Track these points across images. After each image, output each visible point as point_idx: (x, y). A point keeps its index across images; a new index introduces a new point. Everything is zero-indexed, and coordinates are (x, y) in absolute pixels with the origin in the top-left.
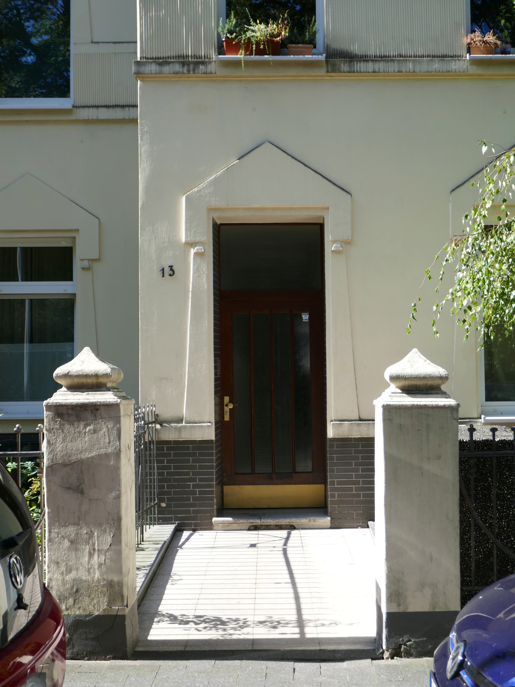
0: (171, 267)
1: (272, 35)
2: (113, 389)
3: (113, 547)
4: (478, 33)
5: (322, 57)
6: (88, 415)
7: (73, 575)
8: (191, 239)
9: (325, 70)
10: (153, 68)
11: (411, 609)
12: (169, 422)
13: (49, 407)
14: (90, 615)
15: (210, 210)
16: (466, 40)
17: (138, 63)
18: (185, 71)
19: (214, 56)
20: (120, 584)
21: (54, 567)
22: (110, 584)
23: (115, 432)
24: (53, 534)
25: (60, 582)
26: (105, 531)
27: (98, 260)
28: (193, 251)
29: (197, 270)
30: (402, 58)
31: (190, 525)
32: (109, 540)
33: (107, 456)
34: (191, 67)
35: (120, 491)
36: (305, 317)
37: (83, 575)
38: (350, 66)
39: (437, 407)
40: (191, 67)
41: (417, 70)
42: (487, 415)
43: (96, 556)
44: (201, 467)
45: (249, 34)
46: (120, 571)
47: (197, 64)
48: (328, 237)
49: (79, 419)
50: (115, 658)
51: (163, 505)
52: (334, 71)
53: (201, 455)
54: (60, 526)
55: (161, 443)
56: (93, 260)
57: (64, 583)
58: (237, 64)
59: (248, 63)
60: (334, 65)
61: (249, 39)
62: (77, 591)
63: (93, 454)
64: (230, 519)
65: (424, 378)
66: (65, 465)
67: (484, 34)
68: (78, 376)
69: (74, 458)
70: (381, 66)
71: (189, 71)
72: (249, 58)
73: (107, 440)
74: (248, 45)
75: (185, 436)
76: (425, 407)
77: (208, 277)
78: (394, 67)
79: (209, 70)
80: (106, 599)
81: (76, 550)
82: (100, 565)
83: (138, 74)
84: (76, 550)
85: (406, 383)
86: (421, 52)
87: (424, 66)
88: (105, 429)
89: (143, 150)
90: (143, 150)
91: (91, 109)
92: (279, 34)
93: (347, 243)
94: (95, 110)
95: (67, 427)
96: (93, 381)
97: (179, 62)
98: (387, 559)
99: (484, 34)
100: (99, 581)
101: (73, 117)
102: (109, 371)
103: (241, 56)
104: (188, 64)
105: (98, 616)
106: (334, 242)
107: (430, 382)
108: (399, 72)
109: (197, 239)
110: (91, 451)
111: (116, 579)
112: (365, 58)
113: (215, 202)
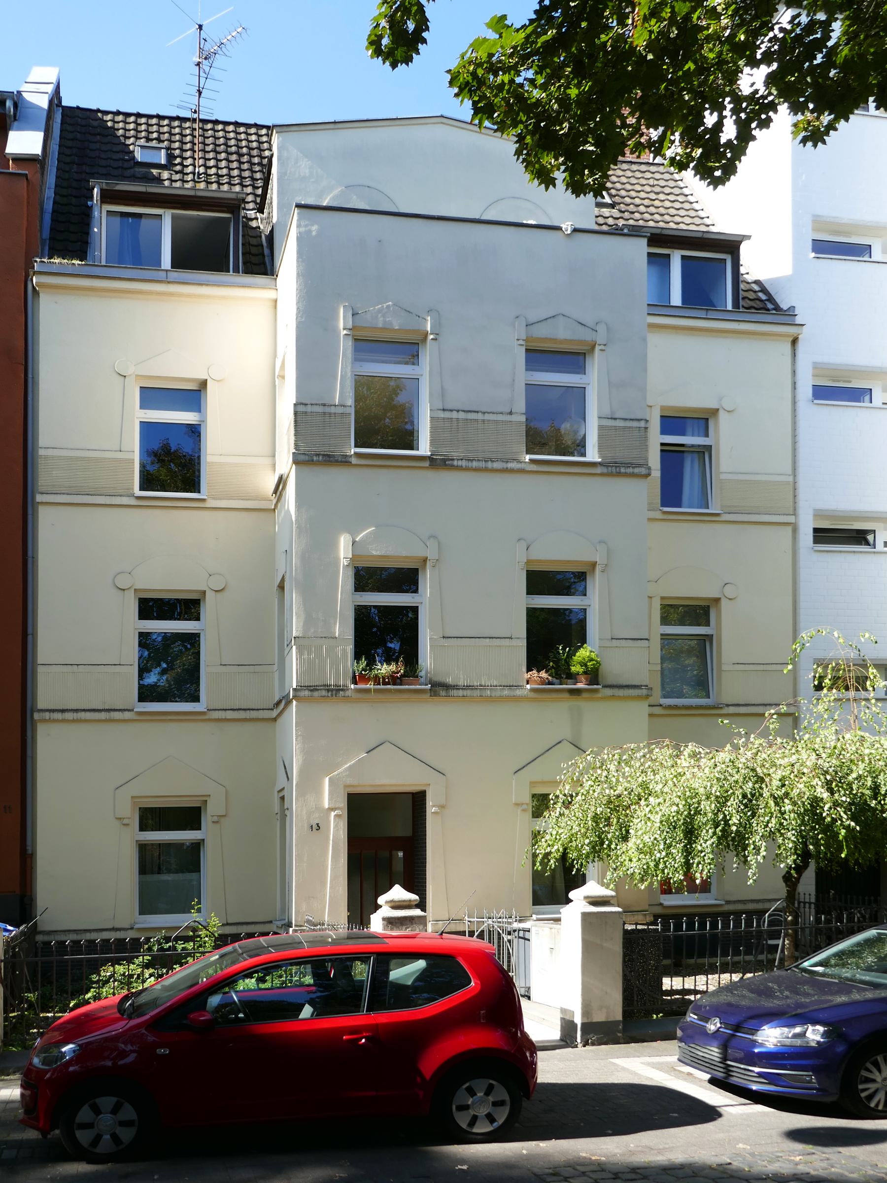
1: (393, 672)
4: (534, 672)
8: (332, 806)
9: (429, 694)
10: (307, 693)
11: (595, 1020)
15: (346, 786)
28: (333, 814)
29: (336, 826)
30: (483, 687)
34: (334, 692)
36: (401, 854)
38: (447, 693)
40: (334, 692)
41: (493, 695)
42: (537, 914)
52: (435, 695)
58: (368, 691)
59: (376, 691)
65: (603, 897)
67: (539, 671)
68: (399, 901)
71: (332, 695)
74: (377, 680)
76: (605, 913)
77: (344, 830)
78: (477, 693)
79: (346, 695)
86: (495, 683)
91: (220, 712)
93: (442, 807)
94: (223, 712)
96: (407, 903)
97: (325, 689)
98: (582, 995)
99: (539, 671)
101: (206, 717)
103: (370, 685)
104: (332, 690)
106: (434, 806)
109: (337, 806)
112: (455, 687)
113: (349, 781)
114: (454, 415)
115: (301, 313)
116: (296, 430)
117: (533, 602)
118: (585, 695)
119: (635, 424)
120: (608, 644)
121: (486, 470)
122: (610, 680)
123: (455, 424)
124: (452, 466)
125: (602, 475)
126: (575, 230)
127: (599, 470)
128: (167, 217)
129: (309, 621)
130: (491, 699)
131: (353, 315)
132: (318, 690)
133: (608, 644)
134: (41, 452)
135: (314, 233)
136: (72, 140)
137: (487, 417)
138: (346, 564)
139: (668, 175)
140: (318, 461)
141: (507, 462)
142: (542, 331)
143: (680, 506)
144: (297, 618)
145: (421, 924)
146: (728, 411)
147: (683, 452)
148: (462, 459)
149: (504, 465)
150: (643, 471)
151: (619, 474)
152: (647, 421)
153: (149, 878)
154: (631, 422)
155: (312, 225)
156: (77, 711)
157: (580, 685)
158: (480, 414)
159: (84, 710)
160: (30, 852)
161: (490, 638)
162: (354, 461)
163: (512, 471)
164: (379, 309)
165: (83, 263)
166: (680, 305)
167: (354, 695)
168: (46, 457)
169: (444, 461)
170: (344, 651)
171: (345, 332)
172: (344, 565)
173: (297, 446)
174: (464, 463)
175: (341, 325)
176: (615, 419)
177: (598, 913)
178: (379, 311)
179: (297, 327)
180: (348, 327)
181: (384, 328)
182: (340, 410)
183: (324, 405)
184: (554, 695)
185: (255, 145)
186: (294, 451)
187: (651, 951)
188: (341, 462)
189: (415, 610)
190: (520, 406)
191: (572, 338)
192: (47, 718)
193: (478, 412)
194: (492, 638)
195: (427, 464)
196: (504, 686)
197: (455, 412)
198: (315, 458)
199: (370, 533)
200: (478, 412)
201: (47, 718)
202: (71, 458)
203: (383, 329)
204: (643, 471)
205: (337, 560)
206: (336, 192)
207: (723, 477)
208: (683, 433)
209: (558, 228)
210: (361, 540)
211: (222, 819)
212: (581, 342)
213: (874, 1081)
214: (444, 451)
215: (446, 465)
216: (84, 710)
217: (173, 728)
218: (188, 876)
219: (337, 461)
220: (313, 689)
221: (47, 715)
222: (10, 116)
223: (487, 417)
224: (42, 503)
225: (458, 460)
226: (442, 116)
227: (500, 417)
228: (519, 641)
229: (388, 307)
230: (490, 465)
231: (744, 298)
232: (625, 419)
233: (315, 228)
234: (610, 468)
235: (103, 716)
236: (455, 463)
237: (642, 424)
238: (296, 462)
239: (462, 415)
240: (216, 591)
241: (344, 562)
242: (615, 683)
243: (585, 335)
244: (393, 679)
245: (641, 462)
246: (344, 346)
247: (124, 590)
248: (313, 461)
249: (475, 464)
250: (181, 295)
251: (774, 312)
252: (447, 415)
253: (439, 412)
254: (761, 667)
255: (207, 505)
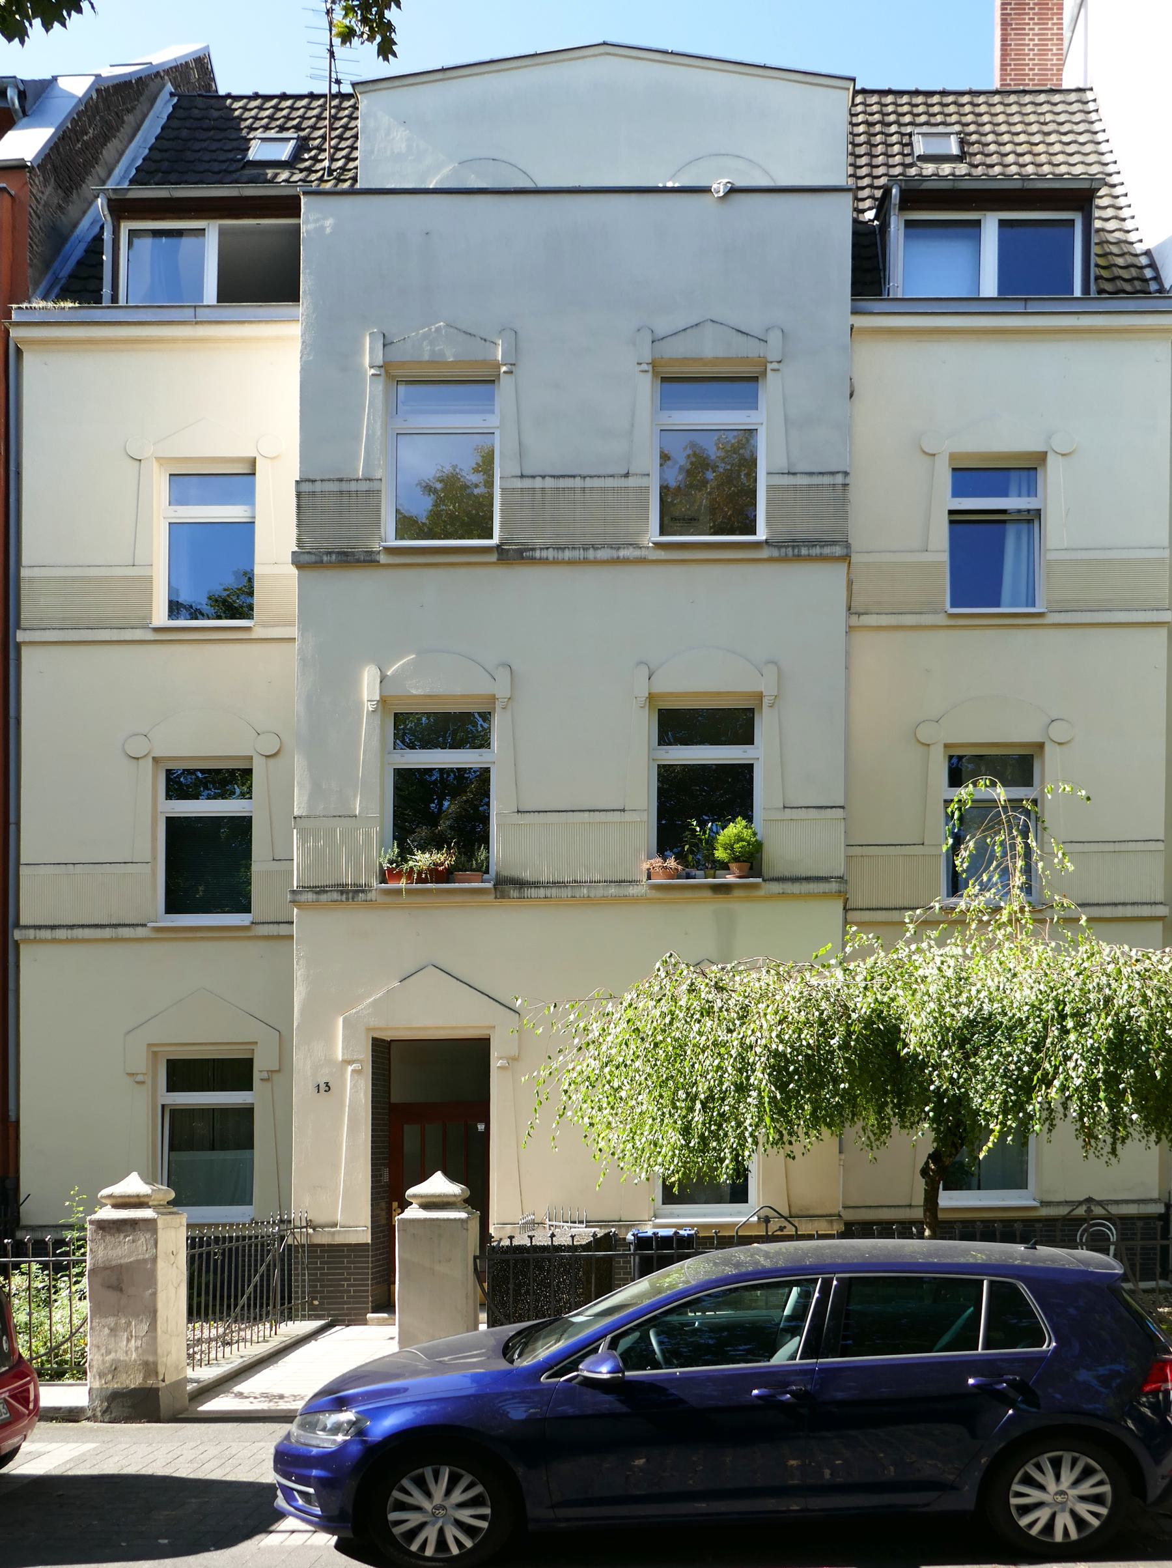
0: (327, 1084)
2: (155, 1207)
3: (149, 1334)
5: (489, 885)
6: (128, 1227)
7: (112, 1356)
8: (348, 1057)
9: (494, 896)
10: (310, 896)
12: (322, 1227)
13: (91, 1222)
14: (127, 1388)
15: (369, 1030)
16: (645, 866)
17: (293, 892)
18: (344, 899)
19: (375, 883)
20: (155, 1364)
21: (94, 1350)
22: (146, 1363)
23: (152, 1242)
24: (94, 1324)
25: (100, 1362)
26: (142, 1320)
27: (278, 1071)
28: (350, 1068)
29: (354, 1086)
31: (343, 1321)
32: (146, 1328)
33: (145, 1261)
34: (350, 895)
35: (156, 1289)
37: (122, 1356)
39: (449, 1220)
40: (350, 895)
41: (592, 895)
43: (133, 1341)
44: (355, 1268)
45: (411, 863)
46: (155, 1352)
47: (357, 892)
48: (494, 1054)
49: (119, 1231)
50: (148, 1422)
51: (316, 1303)
53: (355, 1256)
54: (101, 1317)
55: (313, 1247)
56: (272, 1071)
57: (104, 1362)
58: (398, 892)
59: (409, 891)
60: (502, 892)
61: (411, 868)
62: (115, 1369)
63: (132, 1259)
64: (385, 1315)
65: (439, 1196)
66: (106, 1268)
68: (121, 1197)
69: (114, 1263)
70: (554, 892)
71: (347, 899)
72: (410, 886)
73: (145, 1248)
75: (339, 1240)
76: (437, 1220)
77: (365, 1092)
78: (566, 893)
79: (369, 898)
80: (142, 1375)
81: (115, 1336)
82: (137, 1348)
83: (293, 901)
84: (115, 1336)
85: (423, 1200)
86: (597, 878)
87: (599, 892)
88: (143, 1239)
89: (299, 974)
90: (299, 974)
91: (271, 925)
92: (442, 864)
94: (275, 925)
95: (108, 1238)
96: (136, 1200)
97: (337, 891)
100: (135, 1361)
102: (149, 1192)
103: (403, 884)
104: (347, 892)
105: (135, 1388)
106: (501, 1058)
107: (445, 1200)
108: (572, 897)
109: (355, 1057)
110: (130, 1257)
111: (151, 1359)
112: (536, 885)
113: (374, 1022)
114: (538, 483)
115: (308, 349)
116: (299, 519)
117: (667, 756)
118: (737, 893)
119: (827, 480)
120: (778, 815)
121: (586, 562)
122: (781, 870)
123: (539, 496)
124: (533, 558)
125: (771, 560)
126: (733, 191)
127: (765, 553)
128: (212, 229)
129: (317, 791)
130: (589, 902)
131: (384, 346)
132: (327, 891)
133: (778, 815)
134: (24, 573)
135: (328, 231)
136: (173, 139)
137: (589, 483)
138: (371, 709)
139: (1079, 104)
140: (330, 562)
141: (619, 548)
142: (676, 349)
143: (998, 605)
144: (300, 790)
145: (148, 1230)
146: (1063, 455)
147: (1004, 522)
148: (547, 548)
149: (613, 554)
150: (838, 550)
151: (798, 558)
152: (846, 474)
153: (185, 1156)
154: (820, 477)
155: (325, 218)
156: (72, 927)
157: (730, 879)
158: (578, 479)
159: (83, 926)
160: (13, 1119)
161: (590, 811)
162: (383, 558)
163: (626, 561)
164: (424, 333)
165: (77, 305)
166: (996, 296)
167: (381, 899)
168: (31, 580)
169: (520, 552)
170: (368, 835)
171: (373, 371)
172: (368, 711)
173: (300, 542)
174: (550, 554)
175: (367, 361)
176: (794, 474)
177: (425, 1220)
178: (425, 336)
179: (302, 369)
180: (377, 364)
181: (433, 362)
182: (364, 486)
183: (341, 480)
184: (688, 894)
185: (862, 150)
186: (296, 549)
187: (564, 1280)
188: (365, 561)
189: (484, 775)
190: (648, 461)
191: (726, 355)
192: (32, 937)
193: (574, 477)
194: (594, 811)
195: (493, 558)
196: (611, 882)
197: (539, 480)
198: (325, 558)
199: (408, 663)
200: (574, 477)
201: (32, 937)
202: (65, 579)
203: (431, 363)
204: (838, 550)
205: (359, 704)
206: (446, 171)
207: (1051, 556)
208: (1004, 494)
209: (706, 190)
210: (393, 675)
211: (275, 1077)
212: (745, 360)
213: (1042, 1488)
214: (523, 538)
215: (523, 558)
216: (83, 926)
217: (208, 948)
218: (229, 1155)
219: (358, 561)
220: (319, 890)
221: (31, 933)
222: (16, 111)
223: (589, 483)
224: (25, 643)
225: (541, 549)
226: (605, 44)
227: (610, 483)
228: (634, 814)
229: (438, 330)
230: (591, 554)
231: (1097, 278)
232: (811, 474)
233: (329, 223)
234: (783, 550)
235: (107, 933)
236: (538, 554)
237: (839, 479)
238: (298, 561)
239: (549, 483)
240: (267, 757)
241: (368, 707)
242: (787, 874)
243: (750, 349)
244: (437, 875)
245: (838, 537)
246: (372, 391)
247: (138, 759)
248: (322, 562)
249: (568, 554)
250: (174, 340)
251: (1158, 295)
252: (527, 483)
253: (515, 480)
254: (1111, 847)
255: (254, 635)
